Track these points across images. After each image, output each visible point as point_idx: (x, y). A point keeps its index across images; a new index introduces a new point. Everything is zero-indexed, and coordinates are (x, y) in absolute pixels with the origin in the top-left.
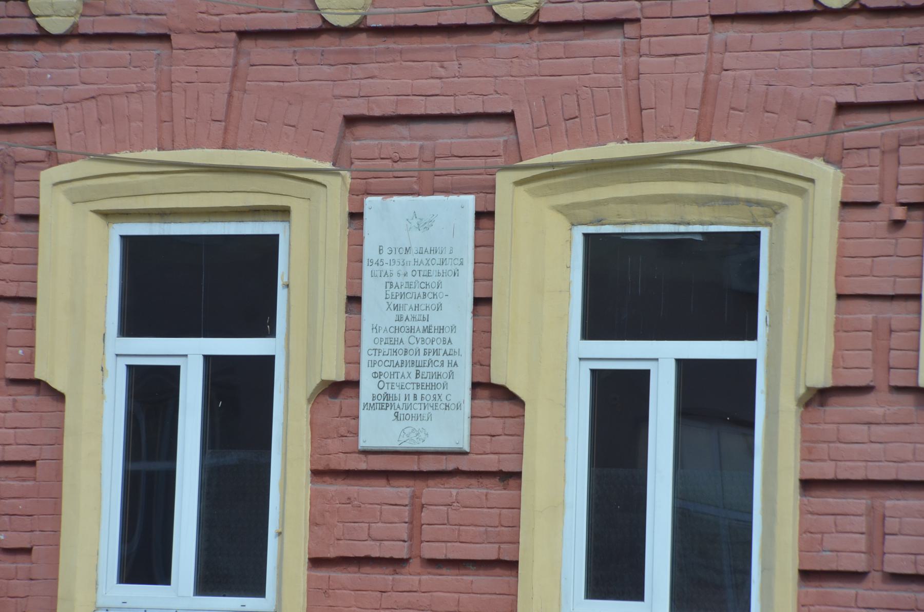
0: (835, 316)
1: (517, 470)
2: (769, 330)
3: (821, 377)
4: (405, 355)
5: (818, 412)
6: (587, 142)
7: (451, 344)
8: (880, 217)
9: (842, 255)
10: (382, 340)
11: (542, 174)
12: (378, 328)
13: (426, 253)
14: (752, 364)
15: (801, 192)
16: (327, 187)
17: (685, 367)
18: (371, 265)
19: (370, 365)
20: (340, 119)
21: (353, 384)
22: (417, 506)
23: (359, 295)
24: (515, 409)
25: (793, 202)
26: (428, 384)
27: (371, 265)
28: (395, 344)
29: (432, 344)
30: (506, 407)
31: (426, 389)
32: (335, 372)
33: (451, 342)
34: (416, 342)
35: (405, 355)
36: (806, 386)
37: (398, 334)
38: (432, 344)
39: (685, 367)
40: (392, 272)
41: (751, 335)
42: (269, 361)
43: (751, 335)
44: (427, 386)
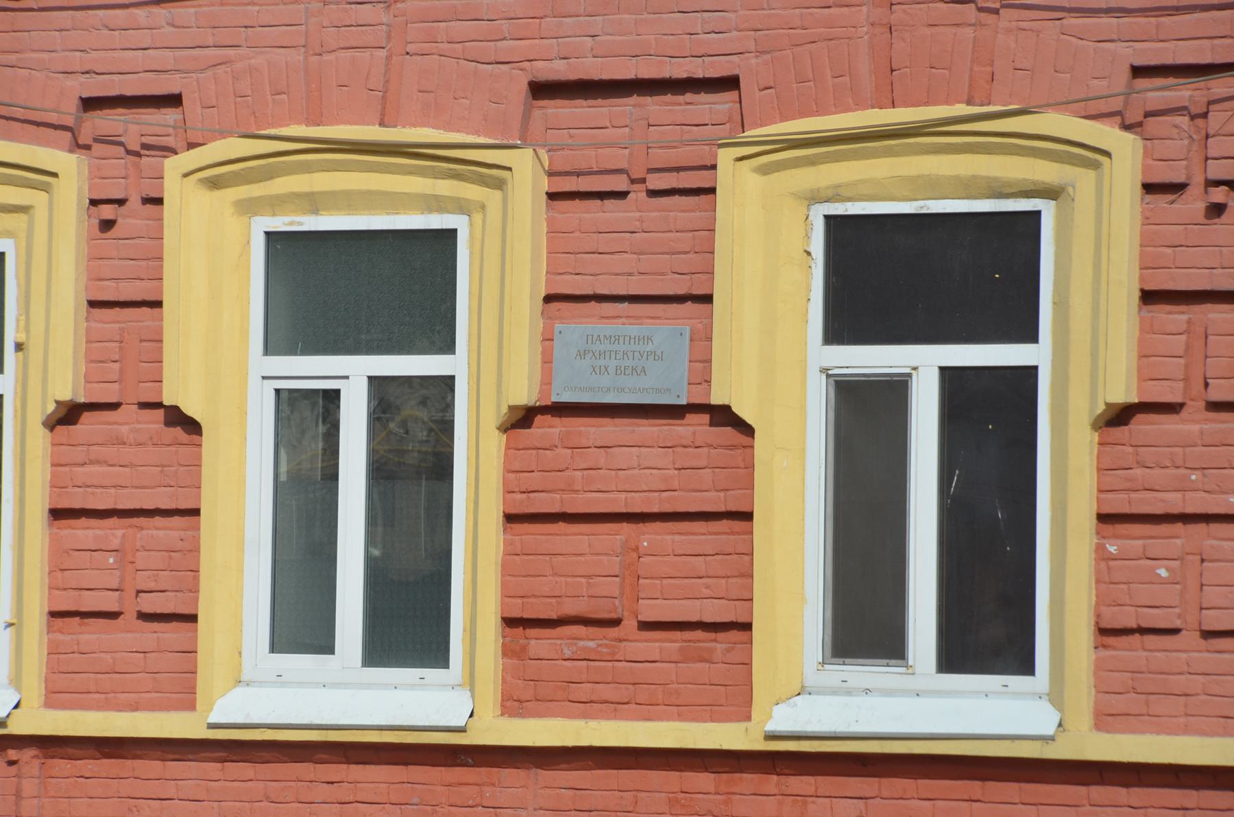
1: (192, 612)
2: (56, 408)
3: (1122, 392)
5: (1120, 432)
6: (629, 116)
8: (1193, 204)
9: (1146, 242)
11: (1056, 150)
14: (1031, 372)
15: (45, 188)
16: (1113, 156)
17: (951, 377)
20: (524, 86)
22: (1184, 496)
23: (159, 299)
24: (743, 439)
25: (493, 197)
30: (728, 433)
37: (611, 334)
39: (951, 377)
41: (1029, 334)
42: (1029, 374)
43: (1029, 334)
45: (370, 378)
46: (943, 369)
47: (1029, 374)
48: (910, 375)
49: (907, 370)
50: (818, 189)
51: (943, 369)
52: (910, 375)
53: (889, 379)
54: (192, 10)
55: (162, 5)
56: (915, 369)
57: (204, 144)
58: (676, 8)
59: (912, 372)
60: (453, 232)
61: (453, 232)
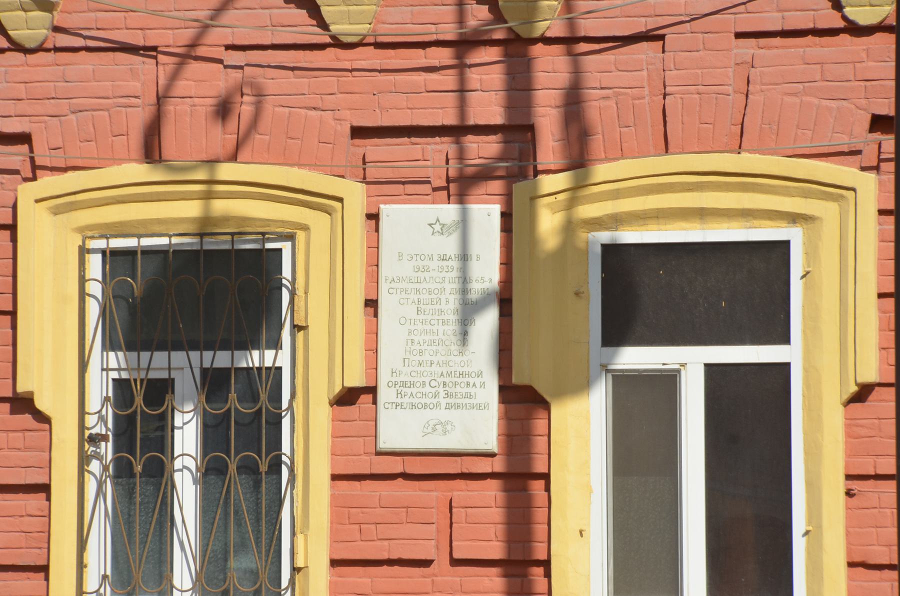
0: (878, 228)
4: (423, 387)
7: (476, 387)
10: (396, 383)
12: (397, 372)
13: (442, 377)
15: (291, 238)
17: (713, 371)
18: (441, 272)
19: (451, 282)
21: (372, 390)
26: (461, 373)
27: (441, 272)
28: (410, 387)
29: (455, 387)
31: (459, 377)
32: (355, 380)
33: (475, 386)
34: (438, 386)
35: (423, 387)
36: (861, 165)
38: (455, 387)
39: (713, 371)
40: (447, 300)
41: (784, 338)
42: (784, 369)
43: (784, 338)
44: (460, 374)
45: (706, 365)
46: (706, 365)
47: (784, 369)
48: (679, 371)
49: (677, 367)
50: (666, 224)
51: (706, 365)
52: (679, 371)
53: (622, 374)
54: (613, 57)
55: (602, 54)
56: (683, 365)
57: (16, 199)
58: (394, 89)
59: (681, 368)
60: (787, 244)
61: (787, 244)
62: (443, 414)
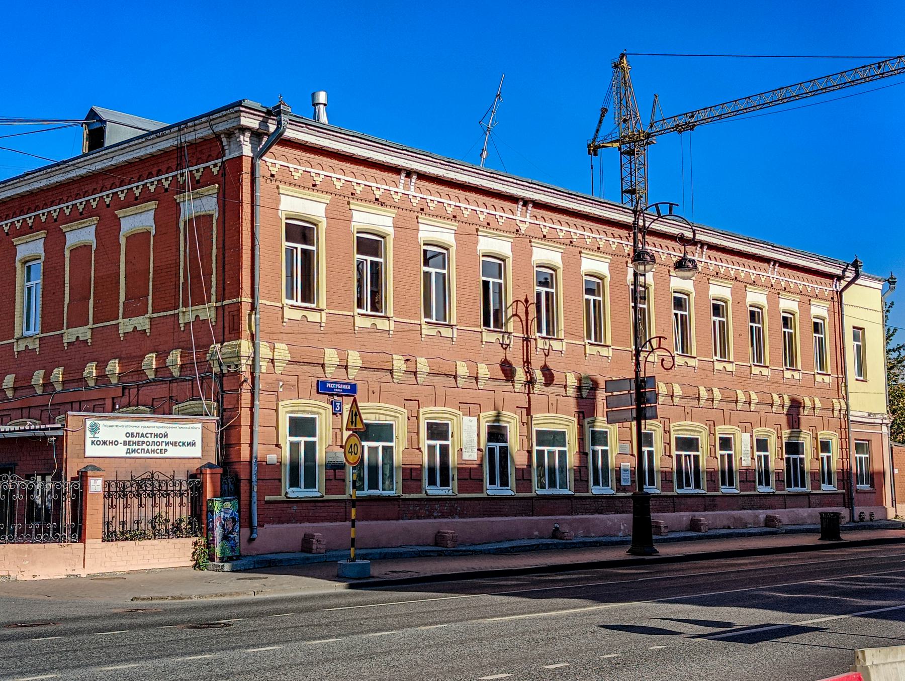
41: (314, 436)
43: (314, 436)
62: (471, 454)
